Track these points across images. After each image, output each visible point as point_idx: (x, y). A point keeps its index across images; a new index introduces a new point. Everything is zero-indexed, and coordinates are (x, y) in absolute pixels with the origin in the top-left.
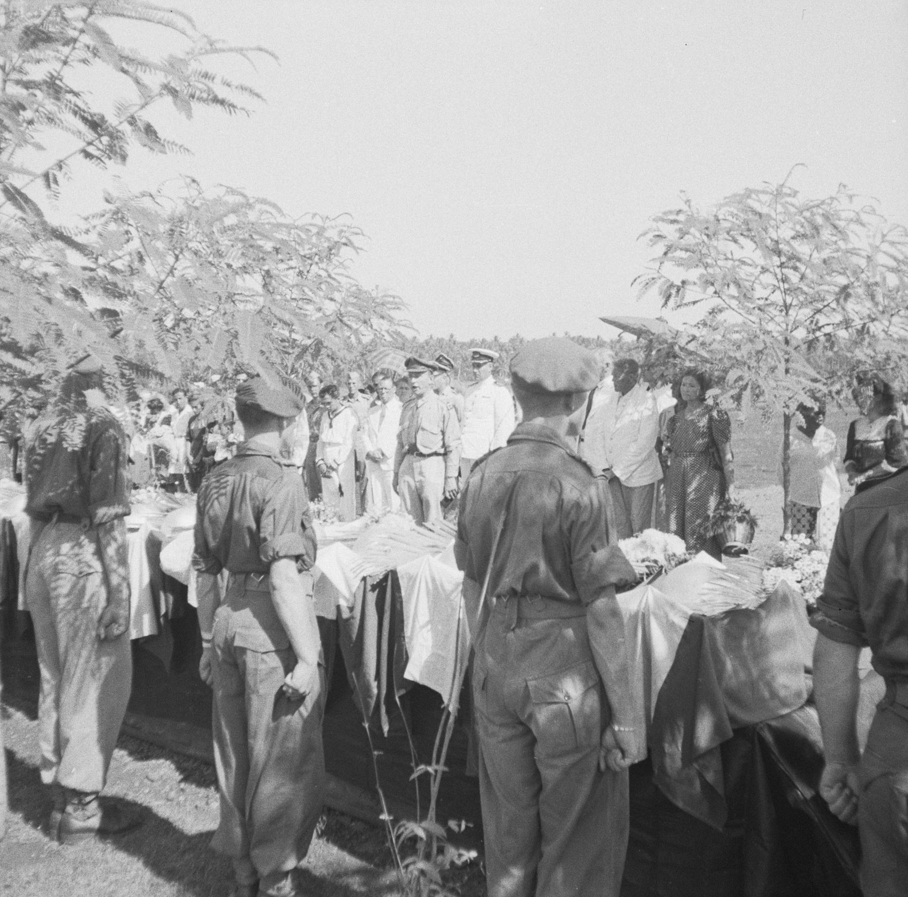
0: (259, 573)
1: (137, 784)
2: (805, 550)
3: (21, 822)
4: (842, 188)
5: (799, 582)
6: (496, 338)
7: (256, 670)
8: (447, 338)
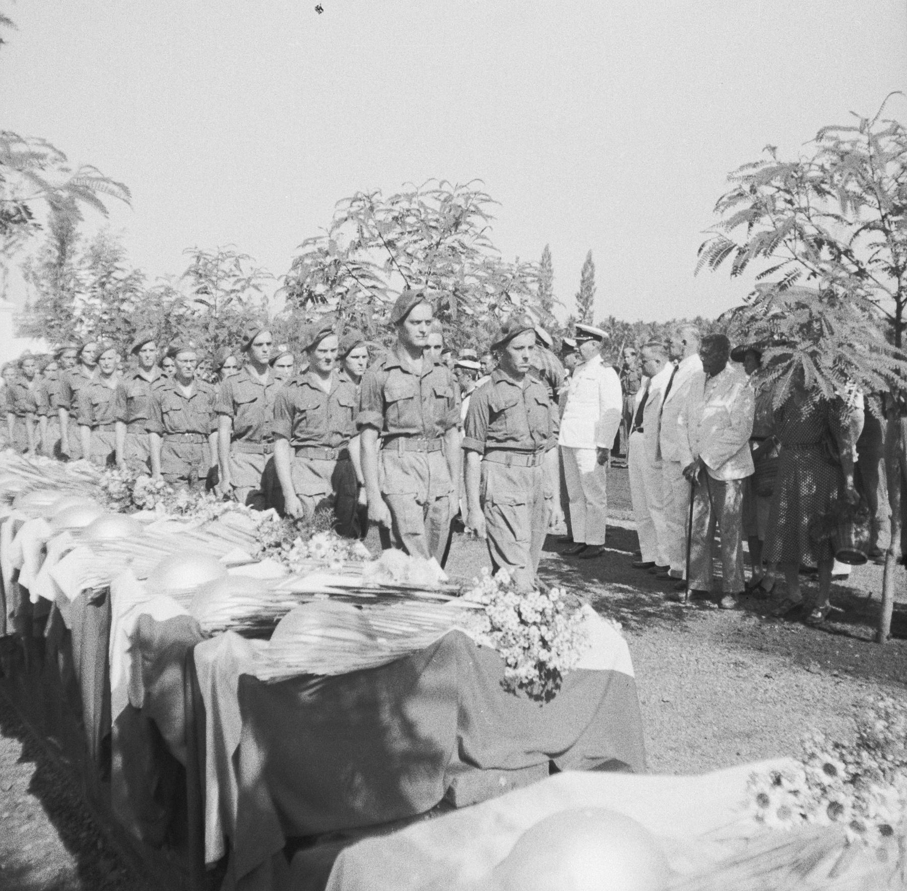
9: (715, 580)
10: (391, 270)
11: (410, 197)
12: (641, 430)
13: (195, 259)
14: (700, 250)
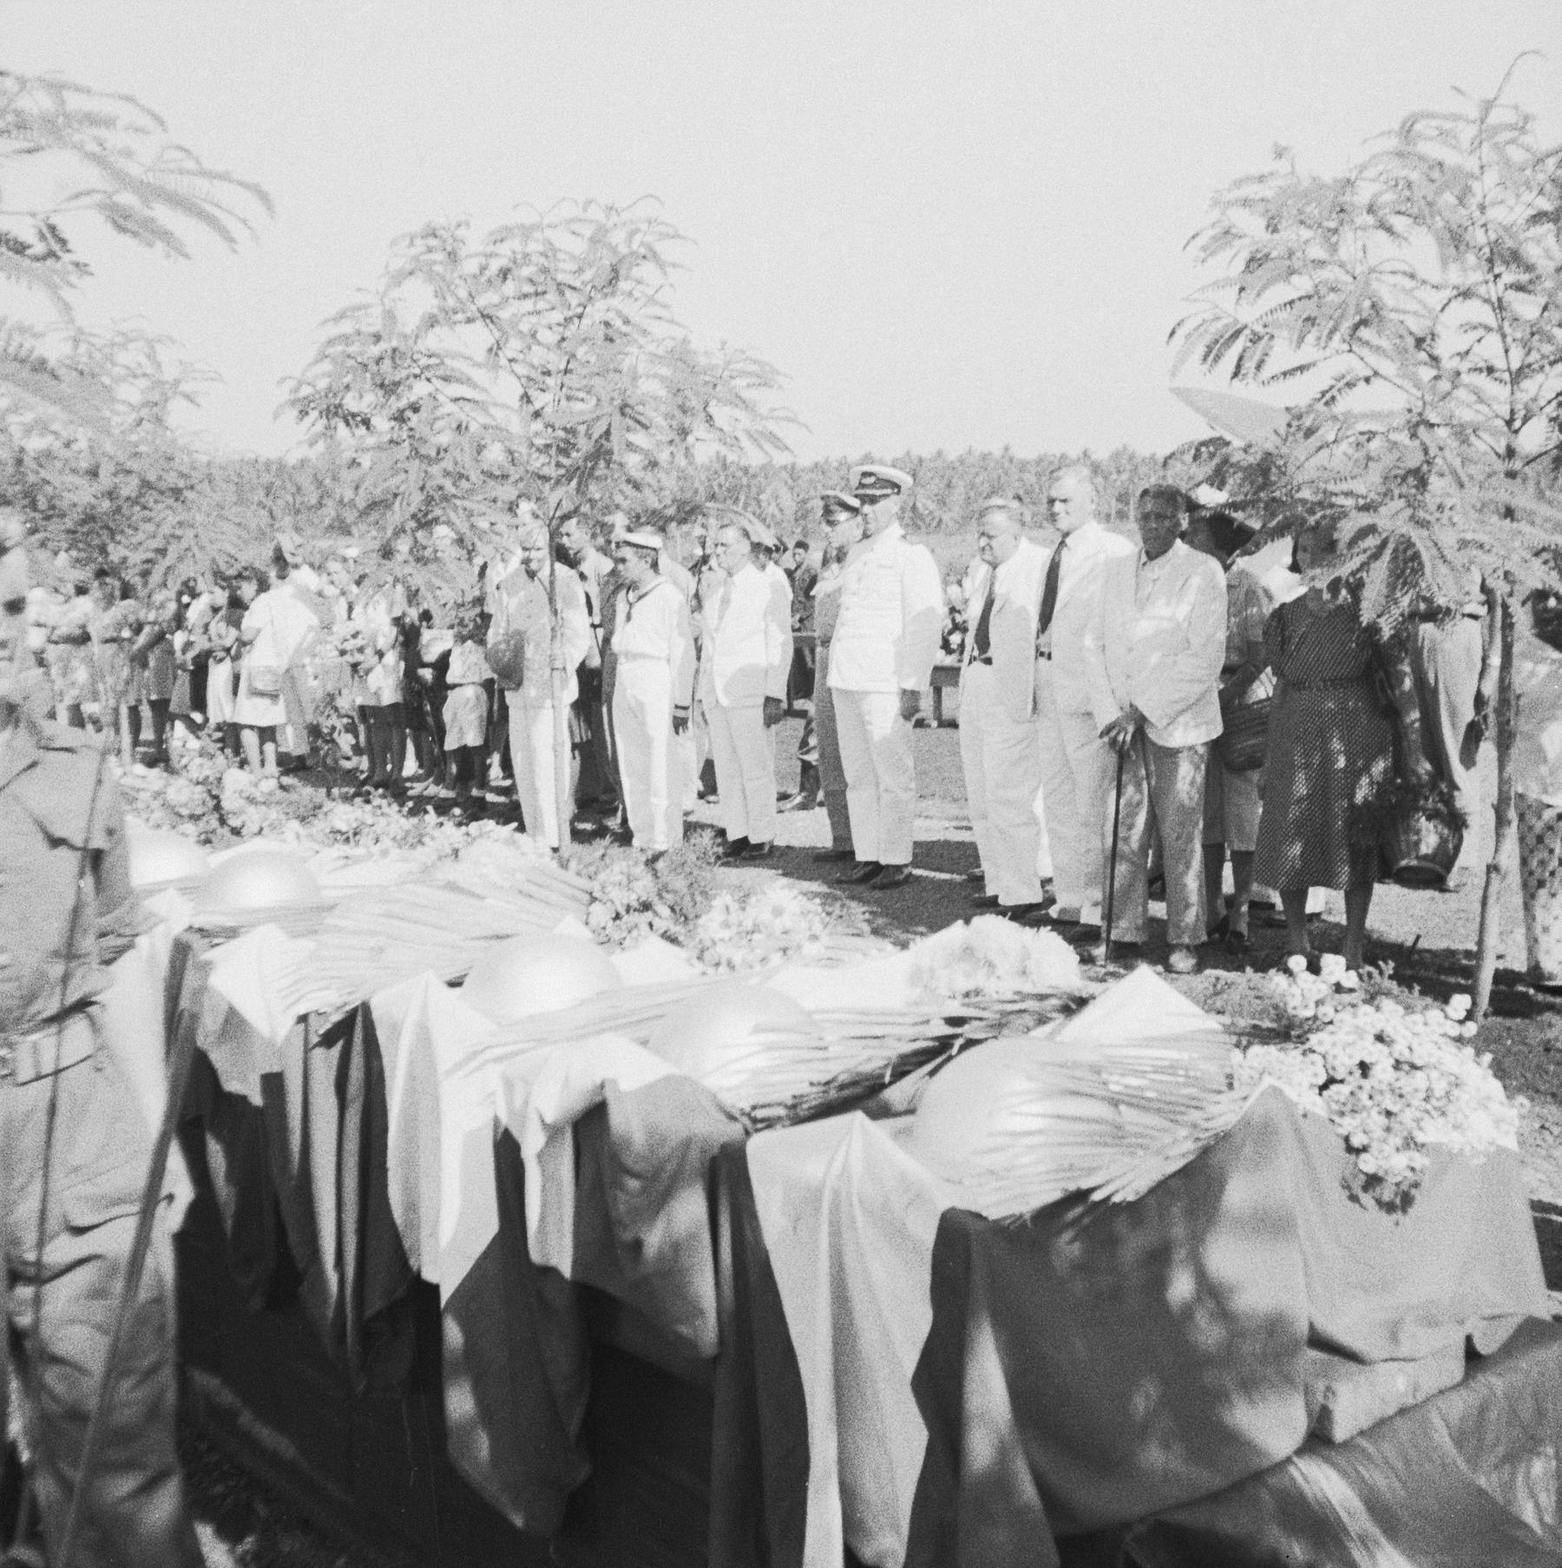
8: (997, 451)
9: (1153, 922)
10: (496, 367)
11: (527, 232)
12: (988, 661)
13: (70, 344)
14: (1173, 333)
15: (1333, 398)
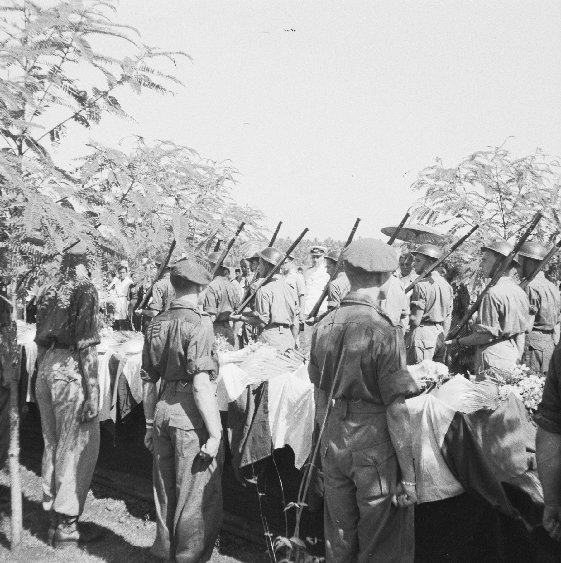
0: (184, 381)
1: (100, 512)
2: (525, 375)
3: (29, 536)
4: (539, 151)
5: (521, 394)
6: (316, 240)
7: (182, 441)
8: (285, 239)
15: (455, 230)
